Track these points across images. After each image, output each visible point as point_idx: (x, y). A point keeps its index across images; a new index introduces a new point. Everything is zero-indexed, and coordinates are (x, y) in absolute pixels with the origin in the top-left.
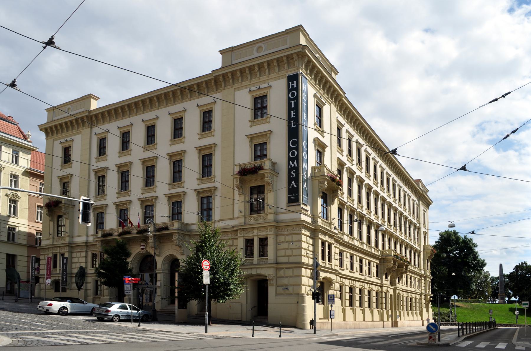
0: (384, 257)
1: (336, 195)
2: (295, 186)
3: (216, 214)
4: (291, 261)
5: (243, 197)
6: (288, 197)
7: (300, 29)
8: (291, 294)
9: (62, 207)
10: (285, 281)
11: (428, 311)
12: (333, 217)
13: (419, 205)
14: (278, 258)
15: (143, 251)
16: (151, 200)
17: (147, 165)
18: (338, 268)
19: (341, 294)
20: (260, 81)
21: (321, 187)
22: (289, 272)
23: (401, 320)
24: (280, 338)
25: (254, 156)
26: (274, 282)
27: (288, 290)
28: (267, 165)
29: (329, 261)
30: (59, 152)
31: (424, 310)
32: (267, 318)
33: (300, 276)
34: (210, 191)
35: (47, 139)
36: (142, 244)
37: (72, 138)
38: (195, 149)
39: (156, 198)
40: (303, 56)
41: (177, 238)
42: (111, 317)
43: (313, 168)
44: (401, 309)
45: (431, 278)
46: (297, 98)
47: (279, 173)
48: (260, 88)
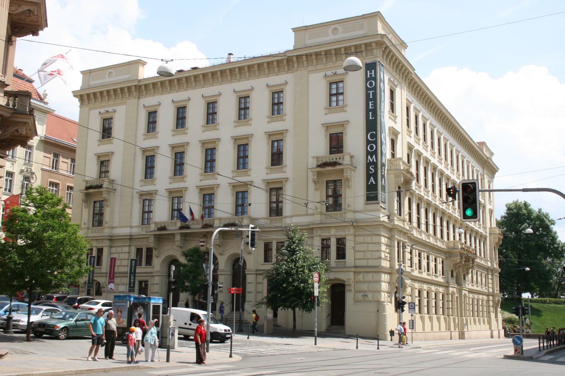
0: (450, 251)
2: (374, 183)
3: (288, 208)
4: (370, 265)
5: (319, 192)
6: (367, 194)
7: (378, 15)
8: (370, 301)
9: (104, 192)
10: (364, 287)
11: (496, 317)
13: (483, 175)
14: (356, 261)
17: (206, 147)
20: (336, 65)
21: (397, 181)
22: (369, 277)
23: (468, 330)
24: (378, 350)
25: (330, 146)
27: (367, 297)
28: (346, 160)
30: (96, 125)
31: (493, 315)
33: (379, 282)
35: (81, 107)
36: (202, 240)
37: (115, 108)
40: (380, 44)
44: (468, 315)
45: (500, 270)
46: (375, 88)
47: (356, 167)
48: (336, 73)
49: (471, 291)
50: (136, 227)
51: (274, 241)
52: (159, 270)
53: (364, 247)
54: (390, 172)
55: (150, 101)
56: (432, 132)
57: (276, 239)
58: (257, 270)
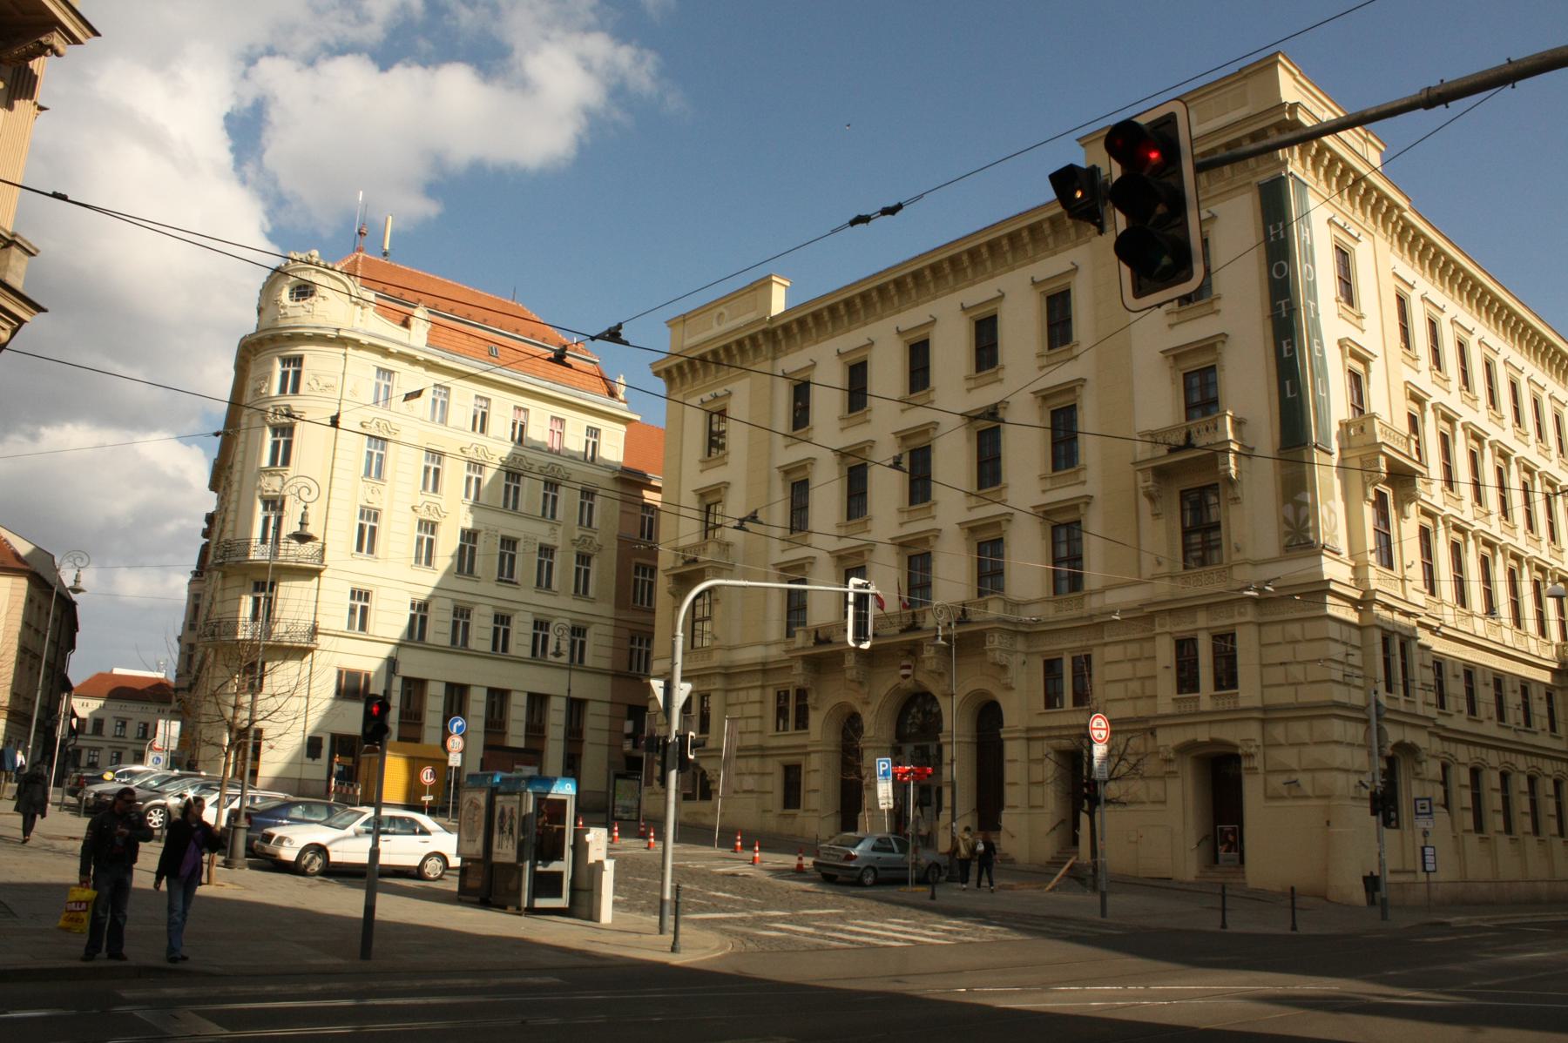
1: (1411, 497)
3: (1094, 572)
5: (1164, 520)
12: (1407, 562)
15: (908, 684)
16: (925, 540)
18: (1432, 712)
19: (1446, 792)
24: (1294, 933)
26: (1257, 762)
29: (1406, 693)
30: (695, 426)
32: (1243, 873)
34: (1076, 507)
36: (905, 663)
37: (729, 387)
38: (1032, 396)
39: (937, 533)
41: (996, 642)
42: (857, 873)
43: (1345, 426)
49: (860, 633)
50: (776, 643)
51: (1065, 653)
52: (819, 739)
53: (1284, 653)
54: (1347, 454)
55: (793, 361)
56: (1535, 401)
57: (1069, 650)
58: (1029, 730)
